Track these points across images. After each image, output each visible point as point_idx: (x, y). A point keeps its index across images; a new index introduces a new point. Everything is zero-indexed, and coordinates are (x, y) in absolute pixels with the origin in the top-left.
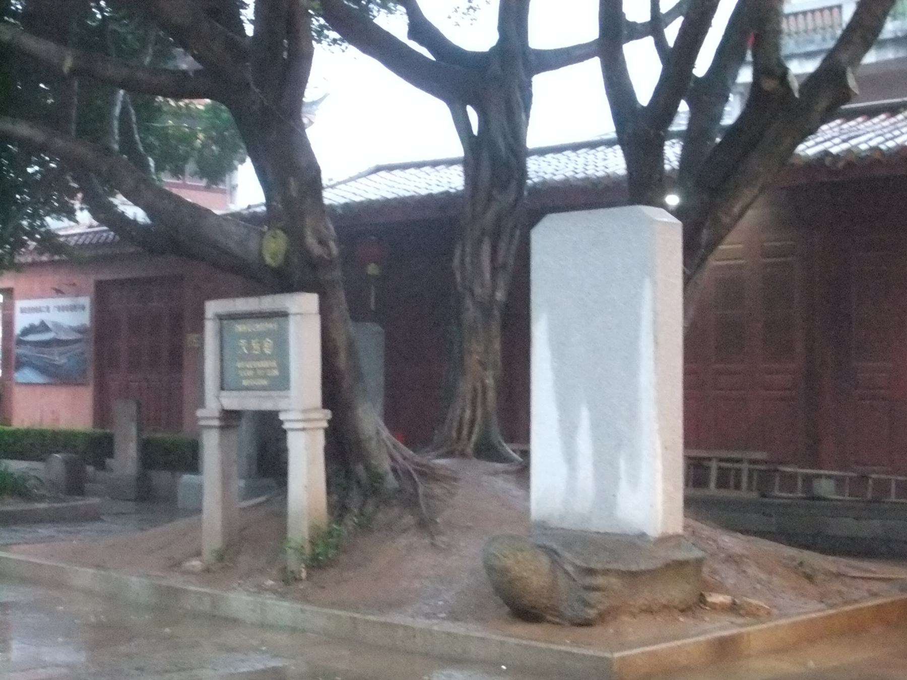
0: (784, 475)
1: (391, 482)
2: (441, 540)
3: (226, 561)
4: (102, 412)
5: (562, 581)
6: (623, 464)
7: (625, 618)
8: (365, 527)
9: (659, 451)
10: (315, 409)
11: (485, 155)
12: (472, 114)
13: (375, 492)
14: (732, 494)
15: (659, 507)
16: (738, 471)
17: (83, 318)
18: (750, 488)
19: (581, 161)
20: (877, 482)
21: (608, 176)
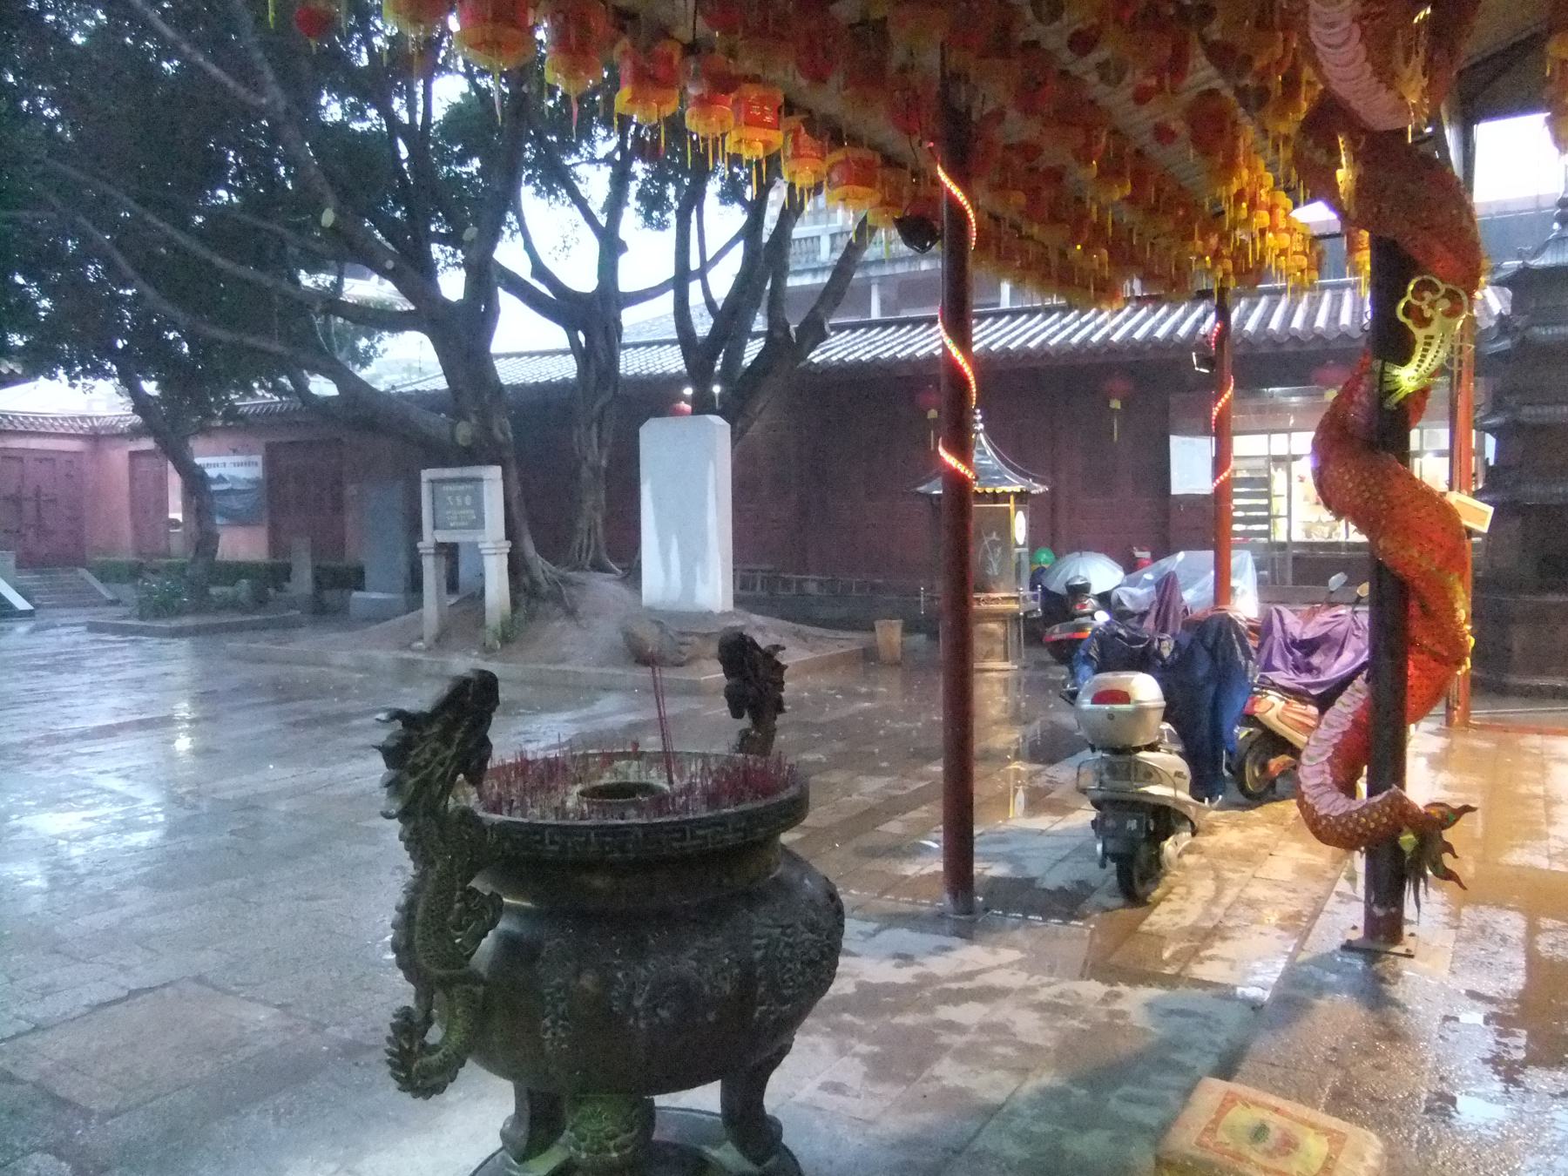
1: (545, 587)
2: (583, 622)
3: (442, 639)
4: (275, 545)
6: (698, 569)
7: (704, 662)
8: (531, 617)
12: (582, 337)
17: (256, 472)
19: (643, 358)
21: (664, 373)
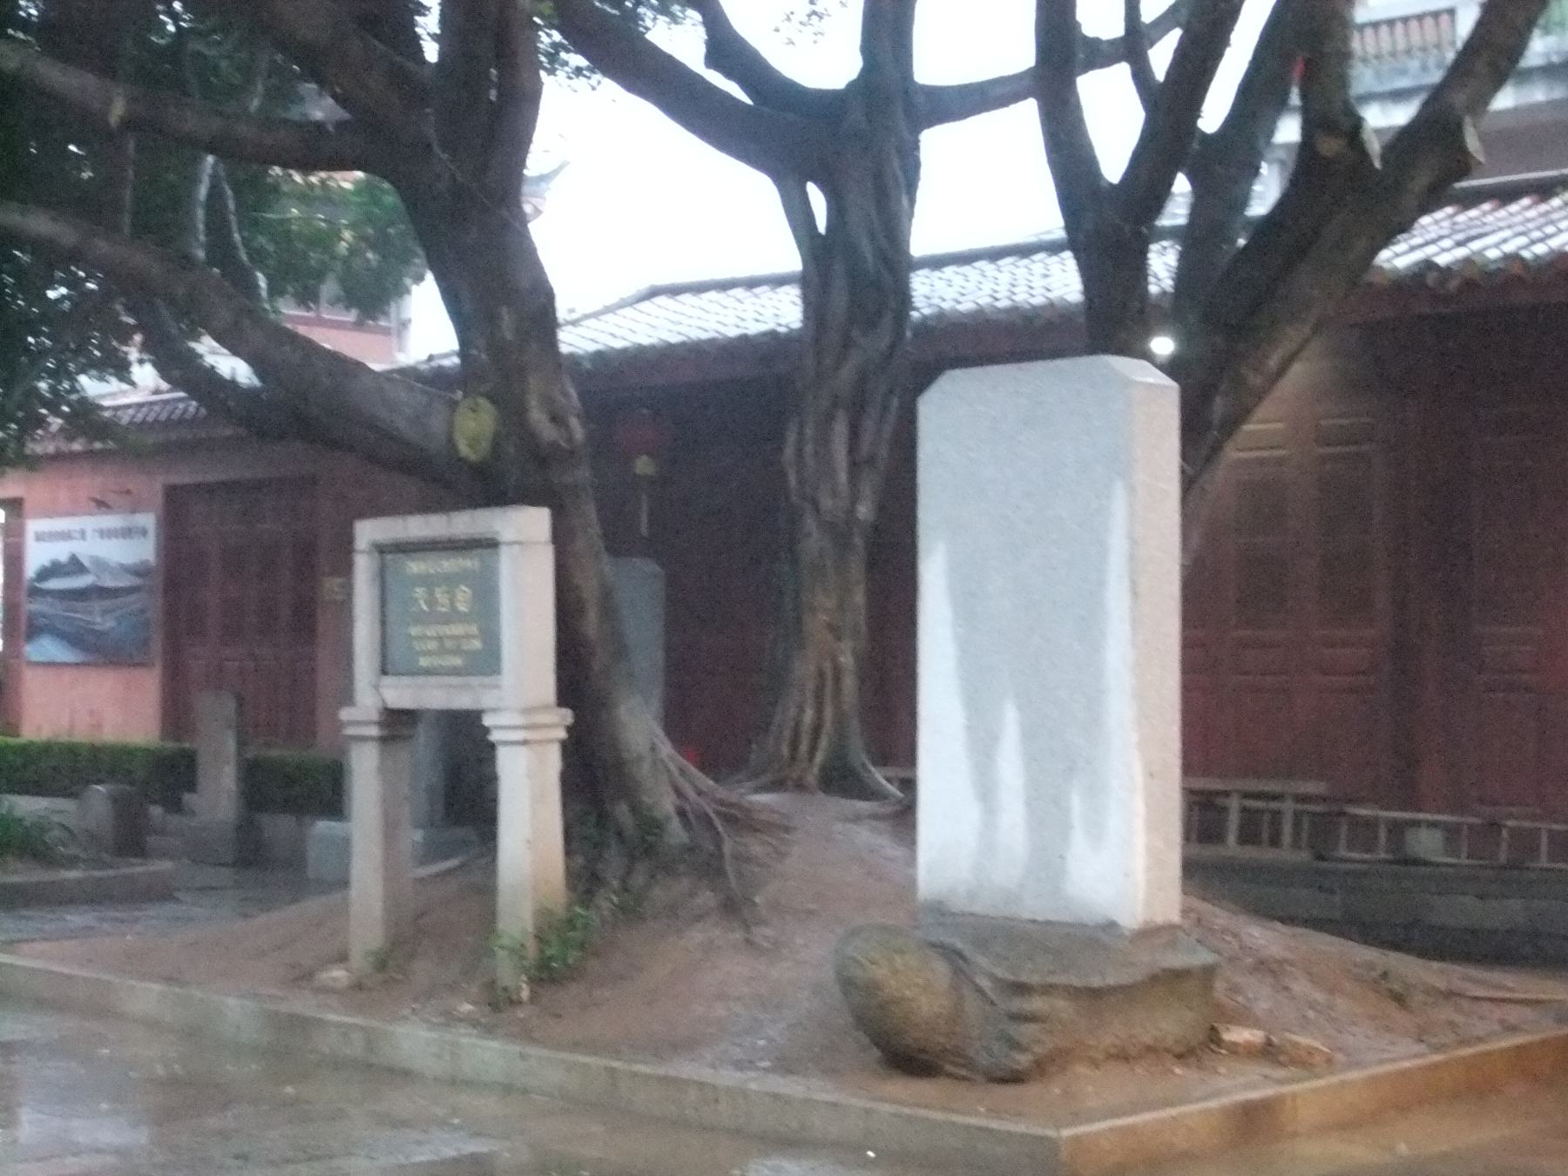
0: (1356, 822)
1: (676, 833)
2: (762, 933)
3: (391, 970)
4: (176, 713)
5: (972, 1005)
6: (1076, 803)
7: (1081, 1069)
8: (631, 911)
9: (1139, 779)
10: (545, 708)
11: (839, 267)
12: (817, 198)
13: (649, 851)
14: (1266, 854)
15: (1140, 877)
16: (1277, 814)
17: (143, 550)
18: (1296, 845)
19: (1005, 278)
20: (1516, 834)
21: (1051, 305)
